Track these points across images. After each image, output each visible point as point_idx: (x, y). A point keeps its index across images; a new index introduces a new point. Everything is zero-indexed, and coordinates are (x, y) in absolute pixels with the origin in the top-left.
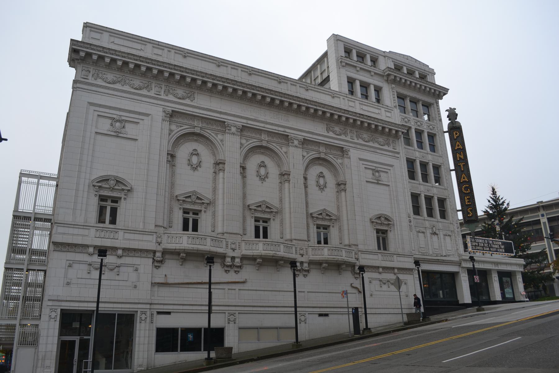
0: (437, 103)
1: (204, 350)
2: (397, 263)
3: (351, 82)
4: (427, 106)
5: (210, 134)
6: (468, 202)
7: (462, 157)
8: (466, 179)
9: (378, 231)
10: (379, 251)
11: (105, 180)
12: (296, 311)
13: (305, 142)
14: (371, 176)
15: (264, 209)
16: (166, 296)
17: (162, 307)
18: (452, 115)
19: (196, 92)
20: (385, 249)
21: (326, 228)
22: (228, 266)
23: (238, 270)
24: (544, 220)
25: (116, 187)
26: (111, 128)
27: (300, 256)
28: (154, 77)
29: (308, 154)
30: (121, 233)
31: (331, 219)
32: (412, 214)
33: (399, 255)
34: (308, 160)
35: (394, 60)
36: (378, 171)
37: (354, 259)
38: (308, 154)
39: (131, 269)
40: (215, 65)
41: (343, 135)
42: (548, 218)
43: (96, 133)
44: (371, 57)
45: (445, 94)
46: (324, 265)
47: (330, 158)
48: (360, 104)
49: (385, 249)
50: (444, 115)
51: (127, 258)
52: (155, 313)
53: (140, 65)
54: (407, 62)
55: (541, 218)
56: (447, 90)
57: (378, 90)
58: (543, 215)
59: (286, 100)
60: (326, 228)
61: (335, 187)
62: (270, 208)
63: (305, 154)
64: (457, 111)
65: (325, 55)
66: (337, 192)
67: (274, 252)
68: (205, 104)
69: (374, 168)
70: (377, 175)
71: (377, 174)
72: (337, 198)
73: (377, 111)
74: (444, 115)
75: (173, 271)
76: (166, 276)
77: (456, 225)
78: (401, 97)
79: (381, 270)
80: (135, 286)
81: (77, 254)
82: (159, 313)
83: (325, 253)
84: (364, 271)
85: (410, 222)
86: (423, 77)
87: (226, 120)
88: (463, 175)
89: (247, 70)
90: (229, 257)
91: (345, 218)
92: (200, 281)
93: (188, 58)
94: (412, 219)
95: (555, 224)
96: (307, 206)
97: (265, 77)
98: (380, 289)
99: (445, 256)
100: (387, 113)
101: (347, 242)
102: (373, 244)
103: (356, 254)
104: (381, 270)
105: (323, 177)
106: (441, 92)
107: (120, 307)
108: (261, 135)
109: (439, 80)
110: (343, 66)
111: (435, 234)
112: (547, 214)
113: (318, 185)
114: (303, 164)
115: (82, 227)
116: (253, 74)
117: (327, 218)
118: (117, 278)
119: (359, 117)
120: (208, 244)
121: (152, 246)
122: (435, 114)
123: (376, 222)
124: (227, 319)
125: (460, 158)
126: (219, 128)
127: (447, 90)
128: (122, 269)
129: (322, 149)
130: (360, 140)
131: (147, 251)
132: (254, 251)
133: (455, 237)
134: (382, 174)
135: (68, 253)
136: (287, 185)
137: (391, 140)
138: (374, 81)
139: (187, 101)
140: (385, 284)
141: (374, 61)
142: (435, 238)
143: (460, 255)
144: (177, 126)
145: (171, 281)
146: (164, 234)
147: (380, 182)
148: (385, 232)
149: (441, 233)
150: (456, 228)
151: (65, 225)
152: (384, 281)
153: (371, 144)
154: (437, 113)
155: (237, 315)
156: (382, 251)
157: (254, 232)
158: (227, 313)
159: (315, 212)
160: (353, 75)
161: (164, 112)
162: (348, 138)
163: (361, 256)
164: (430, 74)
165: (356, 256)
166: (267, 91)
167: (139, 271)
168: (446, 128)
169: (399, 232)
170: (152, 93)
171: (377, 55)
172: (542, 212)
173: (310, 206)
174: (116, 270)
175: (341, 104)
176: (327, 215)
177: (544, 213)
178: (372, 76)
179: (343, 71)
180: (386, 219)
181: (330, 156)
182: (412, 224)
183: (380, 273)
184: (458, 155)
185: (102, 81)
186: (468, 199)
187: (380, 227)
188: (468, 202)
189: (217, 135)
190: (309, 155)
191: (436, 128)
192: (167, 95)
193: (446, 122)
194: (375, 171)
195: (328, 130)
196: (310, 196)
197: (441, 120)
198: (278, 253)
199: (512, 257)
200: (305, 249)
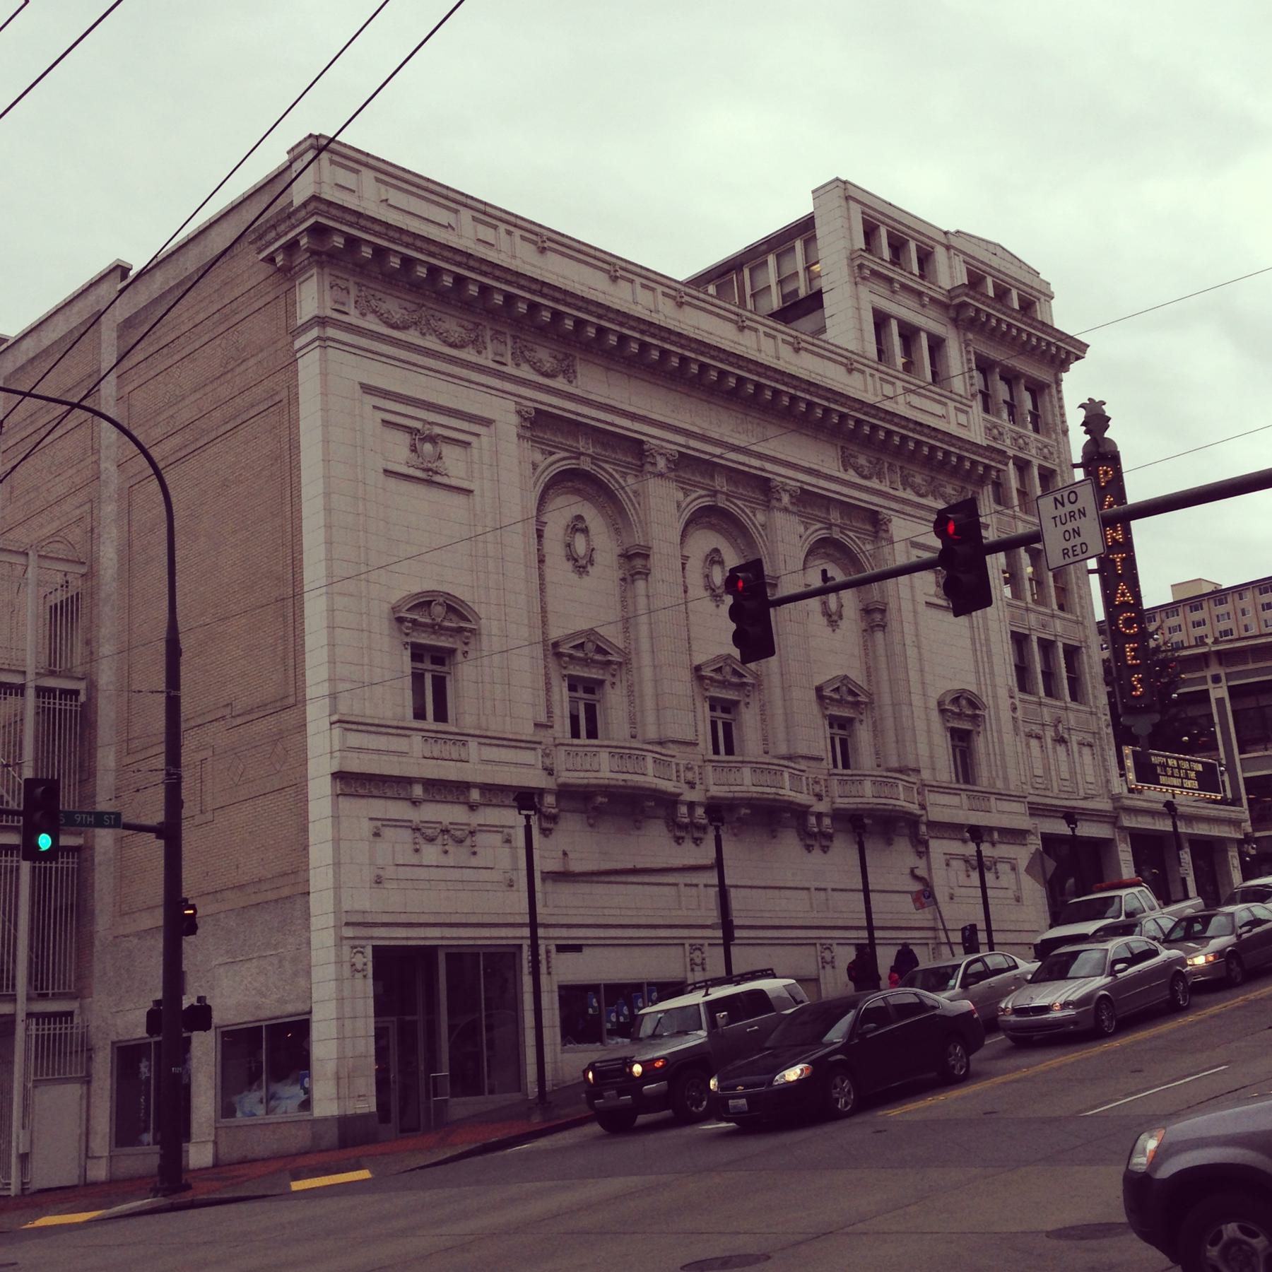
0: (1058, 382)
2: (477, 765)
3: (881, 320)
4: (1037, 389)
5: (611, 475)
6: (1134, 658)
7: (1119, 537)
8: (1129, 598)
9: (418, 653)
11: (424, 603)
12: (534, 937)
13: (807, 500)
15: (590, 655)
16: (561, 905)
17: (564, 933)
18: (1096, 419)
19: (578, 356)
21: (592, 686)
22: (683, 827)
23: (551, 826)
24: (1219, 692)
25: (446, 624)
26: (417, 462)
27: (686, 786)
28: (356, 265)
29: (686, 495)
30: (747, 771)
31: (609, 663)
32: (1016, 689)
33: (1001, 796)
34: (546, 477)
35: (969, 260)
36: (432, 439)
37: (916, 806)
38: (686, 495)
39: (497, 839)
40: (606, 276)
41: (412, 331)
42: (1230, 688)
43: (386, 471)
44: (890, 235)
45: (1078, 358)
46: (600, 799)
47: (738, 507)
48: (474, 219)
50: (1075, 418)
51: (489, 811)
52: (553, 949)
53: (468, 278)
54: (995, 262)
55: (1210, 685)
56: (1083, 347)
57: (936, 345)
58: (1216, 679)
59: (768, 383)
60: (592, 686)
61: (615, 565)
62: (606, 653)
63: (538, 457)
64: (1108, 410)
65: (804, 229)
66: (623, 580)
67: (773, 790)
68: (602, 393)
69: (418, 425)
70: (427, 447)
71: (428, 447)
72: (623, 600)
73: (938, 409)
74: (1075, 418)
75: (575, 843)
76: (565, 854)
77: (1104, 718)
78: (984, 366)
79: (475, 795)
80: (379, 877)
81: (390, 803)
82: (561, 949)
83: (602, 769)
84: (722, 820)
85: (1014, 709)
86: (1027, 305)
87: (644, 438)
88: (1122, 587)
89: (605, 266)
90: (683, 803)
91: (886, 699)
92: (630, 866)
93: (549, 253)
94: (1017, 703)
95: (1250, 703)
96: (544, 623)
97: (711, 313)
98: (414, 859)
99: (1085, 798)
100: (480, 227)
101: (652, 733)
102: (944, 771)
103: (546, 755)
104: (475, 795)
105: (585, 531)
106: (1065, 352)
107: (404, 935)
108: (712, 478)
109: (1064, 316)
110: (864, 278)
111: (1061, 740)
112: (1229, 676)
113: (572, 557)
114: (535, 484)
115: (394, 731)
116: (690, 304)
117: (598, 657)
119: (913, 431)
120: (650, 771)
121: (534, 779)
122: (1054, 415)
123: (414, 621)
124: (688, 960)
125: (1114, 539)
126: (629, 460)
127: (1083, 347)
128: (481, 838)
129: (720, 483)
130: (371, 317)
132: (733, 788)
133: (1103, 749)
134: (449, 452)
135: (371, 800)
136: (879, 635)
137: (886, 460)
138: (929, 322)
139: (559, 383)
140: (431, 840)
141: (925, 257)
142: (1061, 749)
143: (1116, 798)
144: (543, 452)
145: (576, 867)
146: (556, 746)
147: (438, 478)
148: (441, 657)
149: (1074, 738)
150: (1103, 725)
151: (360, 727)
152: (429, 832)
153: (412, 336)
154: (1057, 410)
155: (706, 948)
157: (449, 705)
158: (687, 946)
159: (707, 663)
161: (518, 412)
162: (884, 487)
163: (932, 798)
164: (1043, 298)
165: (548, 762)
166: (751, 366)
167: (513, 844)
168: (1077, 457)
169: (995, 735)
170: (486, 360)
171: (931, 243)
172: (1215, 669)
173: (552, 618)
174: (468, 842)
175: (866, 391)
176: (851, 692)
177: (1222, 672)
178: (924, 306)
179: (864, 291)
180: (450, 609)
181: (851, 534)
182: (1019, 714)
183: (415, 803)
184: (1119, 537)
185: (377, 321)
186: (1132, 650)
187: (424, 639)
188: (1134, 658)
189: (624, 475)
190: (689, 499)
191: (1055, 456)
192: (363, 315)
193: (1078, 440)
194: (418, 437)
195: (846, 464)
196: (550, 590)
197: (1065, 432)
198: (781, 792)
199: (1215, 802)
200: (822, 782)
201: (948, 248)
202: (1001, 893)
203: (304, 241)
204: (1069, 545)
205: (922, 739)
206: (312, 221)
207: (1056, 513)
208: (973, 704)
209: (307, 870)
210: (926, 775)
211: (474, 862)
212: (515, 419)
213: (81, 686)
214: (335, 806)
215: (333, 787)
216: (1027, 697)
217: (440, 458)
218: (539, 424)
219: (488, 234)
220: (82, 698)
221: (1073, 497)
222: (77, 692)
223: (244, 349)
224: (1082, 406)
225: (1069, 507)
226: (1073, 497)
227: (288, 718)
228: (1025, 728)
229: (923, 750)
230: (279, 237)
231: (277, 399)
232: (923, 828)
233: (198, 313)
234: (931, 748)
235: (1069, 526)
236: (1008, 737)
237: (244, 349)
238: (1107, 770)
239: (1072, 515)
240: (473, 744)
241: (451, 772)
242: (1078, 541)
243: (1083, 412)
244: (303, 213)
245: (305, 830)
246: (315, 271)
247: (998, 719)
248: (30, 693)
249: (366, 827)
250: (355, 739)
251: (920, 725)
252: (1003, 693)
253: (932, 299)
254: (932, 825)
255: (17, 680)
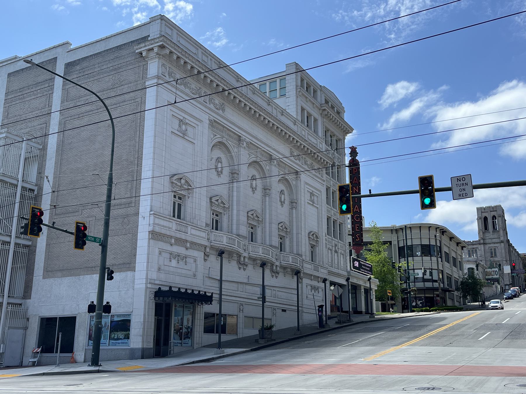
1: (216, 333)
3: (303, 109)
10: (174, 218)
14: (177, 127)
18: (354, 152)
20: (179, 217)
49: (179, 217)
50: (348, 151)
69: (182, 118)
111: (336, 252)
116: (256, 94)
118: (185, 267)
123: (176, 184)
131: (202, 245)
134: (189, 129)
142: (336, 254)
147: (186, 137)
156: (175, 219)
160: (305, 106)
168: (347, 163)
189: (234, 146)
193: (347, 160)
201: (321, 90)
202: (318, 298)
203: (156, 50)
204: (461, 193)
205: (303, 246)
206: (161, 43)
207: (458, 183)
208: (317, 237)
209: (135, 263)
210: (304, 257)
211: (185, 267)
212: (208, 122)
213: (36, 188)
214: (149, 243)
215: (149, 236)
216: (329, 237)
217: (187, 130)
218: (213, 124)
219: (205, 58)
220: (36, 193)
221: (464, 179)
222: (33, 190)
223: (122, 81)
224: (350, 148)
225: (462, 182)
226: (464, 179)
227: (131, 210)
228: (328, 246)
229: (303, 250)
230: (145, 46)
231: (136, 100)
232: (302, 275)
233: (103, 66)
234: (305, 249)
235: (462, 188)
236: (324, 249)
237: (122, 81)
238: (346, 263)
239: (463, 184)
240: (189, 228)
241: (183, 236)
242: (464, 192)
243: (350, 150)
244: (158, 40)
245: (136, 249)
246: (157, 60)
247: (322, 243)
248: (19, 188)
249: (157, 251)
250: (157, 221)
251: (303, 242)
252: (324, 235)
253: (316, 106)
254: (304, 273)
255: (15, 182)
